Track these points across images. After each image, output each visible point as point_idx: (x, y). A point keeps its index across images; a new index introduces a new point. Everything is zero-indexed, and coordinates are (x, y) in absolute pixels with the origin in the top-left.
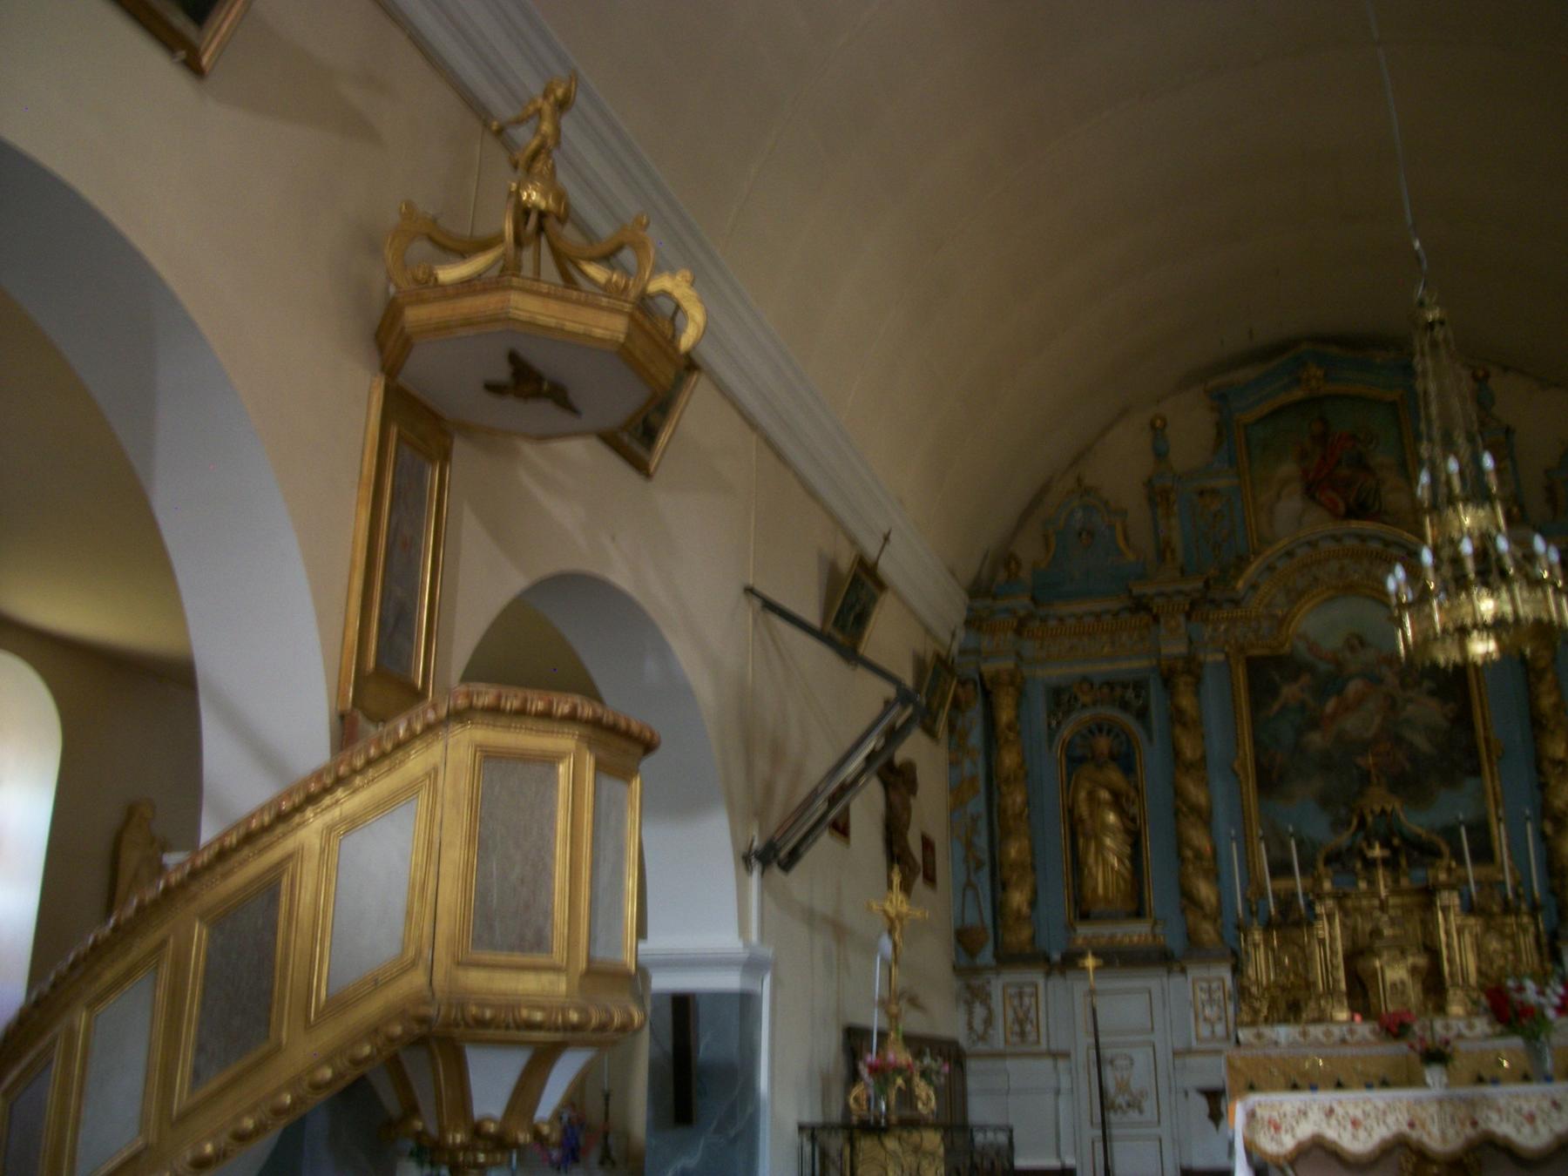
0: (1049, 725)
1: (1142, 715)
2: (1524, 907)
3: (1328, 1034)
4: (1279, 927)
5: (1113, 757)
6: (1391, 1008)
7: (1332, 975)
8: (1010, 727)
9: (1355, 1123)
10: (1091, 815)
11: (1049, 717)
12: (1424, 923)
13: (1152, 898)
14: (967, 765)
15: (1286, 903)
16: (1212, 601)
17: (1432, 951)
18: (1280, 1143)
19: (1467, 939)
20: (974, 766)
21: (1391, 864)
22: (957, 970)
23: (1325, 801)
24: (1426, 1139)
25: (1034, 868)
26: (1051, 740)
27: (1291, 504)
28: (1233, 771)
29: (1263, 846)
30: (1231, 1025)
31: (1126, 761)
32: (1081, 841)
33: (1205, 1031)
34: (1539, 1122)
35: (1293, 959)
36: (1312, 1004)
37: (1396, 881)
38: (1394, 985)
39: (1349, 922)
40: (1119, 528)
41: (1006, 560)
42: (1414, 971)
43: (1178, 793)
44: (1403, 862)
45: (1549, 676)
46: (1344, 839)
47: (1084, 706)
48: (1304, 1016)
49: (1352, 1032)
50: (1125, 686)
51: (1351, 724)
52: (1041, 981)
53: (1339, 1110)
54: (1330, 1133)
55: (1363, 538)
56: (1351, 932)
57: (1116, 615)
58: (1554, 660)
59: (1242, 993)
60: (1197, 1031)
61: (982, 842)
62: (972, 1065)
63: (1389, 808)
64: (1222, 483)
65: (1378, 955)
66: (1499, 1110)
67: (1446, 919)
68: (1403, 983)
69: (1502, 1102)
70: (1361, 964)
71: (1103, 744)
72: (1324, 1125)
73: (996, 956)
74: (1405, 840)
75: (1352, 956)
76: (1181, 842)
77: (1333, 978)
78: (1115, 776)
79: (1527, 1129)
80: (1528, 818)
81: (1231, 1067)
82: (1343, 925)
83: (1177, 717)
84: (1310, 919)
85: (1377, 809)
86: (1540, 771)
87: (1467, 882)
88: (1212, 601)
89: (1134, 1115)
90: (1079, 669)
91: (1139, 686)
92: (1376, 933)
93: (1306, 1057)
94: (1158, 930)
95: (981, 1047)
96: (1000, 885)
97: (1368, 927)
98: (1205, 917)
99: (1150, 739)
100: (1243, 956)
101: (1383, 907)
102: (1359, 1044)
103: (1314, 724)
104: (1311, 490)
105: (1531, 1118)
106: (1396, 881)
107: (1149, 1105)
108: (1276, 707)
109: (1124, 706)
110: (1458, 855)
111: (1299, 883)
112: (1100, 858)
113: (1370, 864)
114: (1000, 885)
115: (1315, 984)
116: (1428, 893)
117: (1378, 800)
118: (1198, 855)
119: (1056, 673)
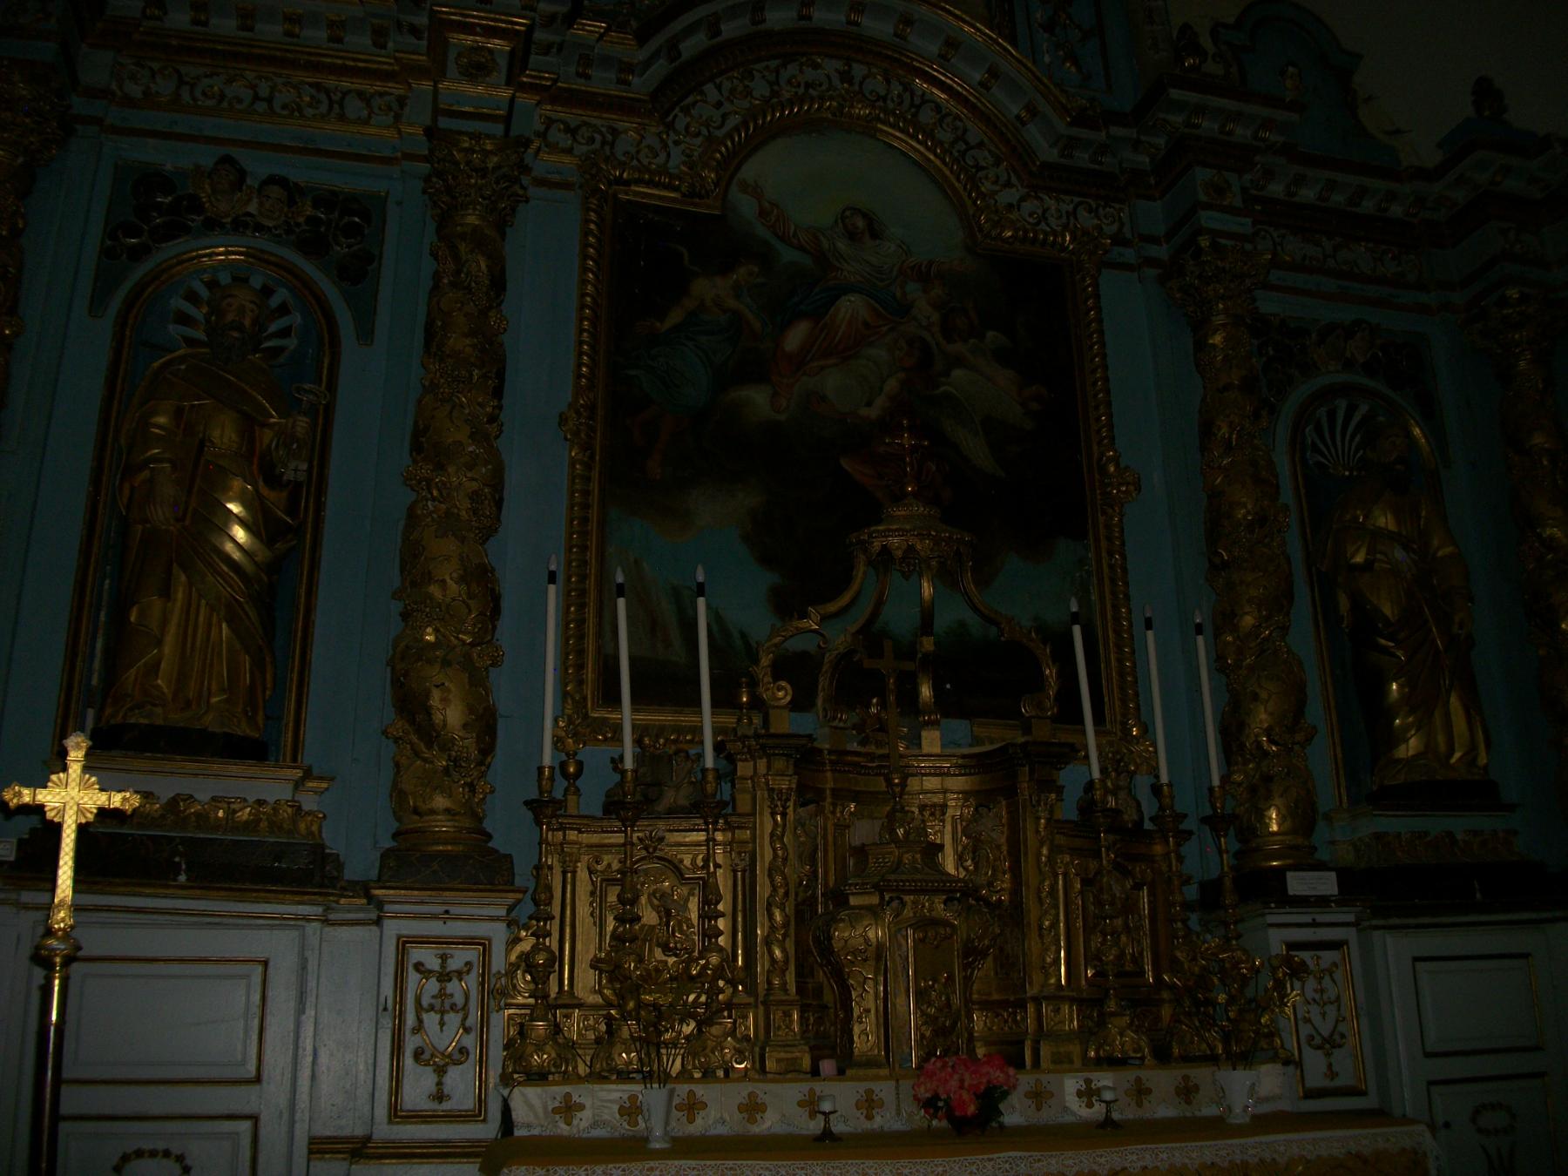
108: (675, 317)
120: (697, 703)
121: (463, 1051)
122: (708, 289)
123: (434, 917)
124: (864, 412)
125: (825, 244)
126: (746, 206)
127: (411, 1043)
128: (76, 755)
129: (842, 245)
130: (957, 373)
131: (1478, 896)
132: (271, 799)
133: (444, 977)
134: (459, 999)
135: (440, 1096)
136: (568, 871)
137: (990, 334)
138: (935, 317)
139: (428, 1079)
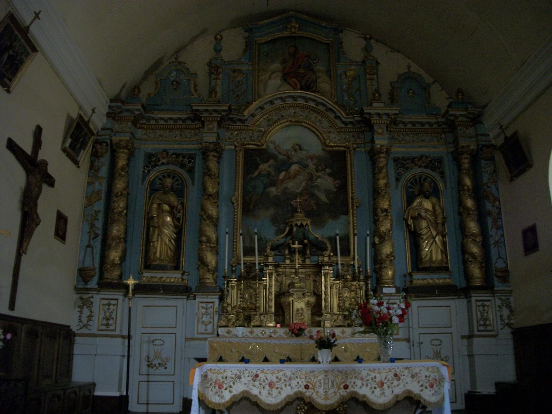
0: (144, 172)
1: (191, 171)
2: (362, 277)
3: (263, 333)
4: (245, 279)
5: (172, 189)
6: (295, 322)
7: (268, 304)
8: (123, 169)
9: (271, 385)
10: (158, 215)
11: (144, 168)
12: (315, 281)
13: (184, 260)
14: (97, 186)
15: (250, 267)
16: (232, 120)
17: (318, 296)
18: (222, 397)
19: (335, 290)
20: (101, 186)
21: (302, 253)
22: (77, 290)
23: (274, 220)
24: (314, 396)
25: (125, 241)
26: (143, 180)
27: (275, 82)
28: (232, 202)
29: (241, 237)
30: (215, 327)
31: (180, 193)
32: (151, 229)
33: (202, 328)
34: (385, 386)
35: (250, 296)
36: (257, 318)
37: (304, 261)
38: (298, 310)
39: (279, 279)
40: (192, 82)
41: (135, 90)
42: (308, 304)
43: (203, 209)
44: (308, 252)
45: (384, 171)
46: (280, 239)
47: (163, 164)
48: (252, 324)
49: (275, 332)
50: (184, 157)
51: (290, 185)
52: (121, 298)
53: (262, 376)
54: (255, 391)
55: (306, 99)
56: (280, 284)
57: (184, 121)
58: (387, 164)
59: (223, 311)
60: (198, 329)
61: (99, 224)
62: (78, 339)
63: (304, 223)
64: (244, 68)
65: (291, 295)
66: (362, 379)
67: (326, 281)
68: (302, 309)
69: (364, 373)
70: (283, 300)
71: (169, 181)
72: (251, 386)
73: (98, 284)
74: (309, 241)
75: (279, 296)
76: (201, 233)
77: (269, 292)
78: (173, 199)
79: (378, 391)
80: (368, 235)
81: (212, 347)
82: (276, 280)
83: (207, 172)
84: (261, 277)
85: (299, 223)
86: (375, 214)
87: (337, 264)
88: (232, 120)
89: (161, 370)
90: (163, 146)
91: (191, 157)
92: (292, 285)
93: (250, 344)
94: (185, 277)
95: (85, 331)
96: (105, 247)
97: (288, 282)
98: (209, 271)
99: (193, 178)
100: (226, 292)
101: (296, 273)
102: (277, 338)
103: (273, 183)
104: (285, 77)
105: (382, 384)
106: (304, 261)
107: (170, 365)
108: (256, 174)
109: (182, 166)
110: (335, 251)
111: (257, 259)
112: (160, 237)
113: (292, 252)
114: (105, 247)
115: (259, 308)
116: (319, 267)
117: (300, 219)
118: (209, 241)
119: (150, 147)
120: (255, 255)
121: (210, 322)
122: (263, 167)
123: (205, 298)
124: (297, 191)
125: (289, 153)
126: (272, 146)
127: (201, 321)
128: (131, 278)
129: (293, 153)
130: (319, 180)
131: (437, 293)
132: (177, 277)
133: (206, 309)
134: (210, 312)
135: (206, 330)
136: (154, 231)
137: (327, 170)
138: (314, 167)
139: (204, 327)
